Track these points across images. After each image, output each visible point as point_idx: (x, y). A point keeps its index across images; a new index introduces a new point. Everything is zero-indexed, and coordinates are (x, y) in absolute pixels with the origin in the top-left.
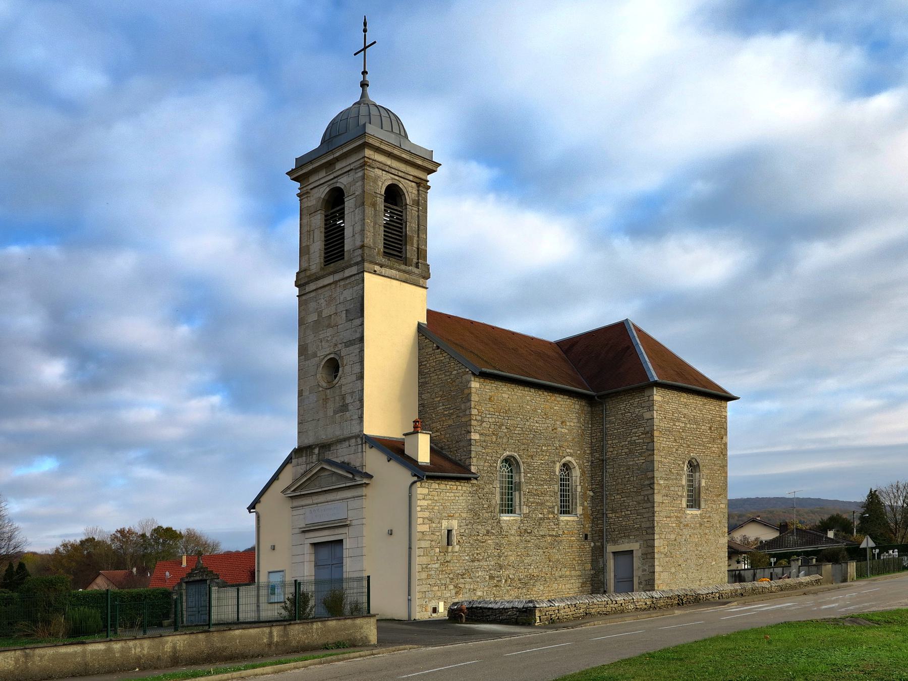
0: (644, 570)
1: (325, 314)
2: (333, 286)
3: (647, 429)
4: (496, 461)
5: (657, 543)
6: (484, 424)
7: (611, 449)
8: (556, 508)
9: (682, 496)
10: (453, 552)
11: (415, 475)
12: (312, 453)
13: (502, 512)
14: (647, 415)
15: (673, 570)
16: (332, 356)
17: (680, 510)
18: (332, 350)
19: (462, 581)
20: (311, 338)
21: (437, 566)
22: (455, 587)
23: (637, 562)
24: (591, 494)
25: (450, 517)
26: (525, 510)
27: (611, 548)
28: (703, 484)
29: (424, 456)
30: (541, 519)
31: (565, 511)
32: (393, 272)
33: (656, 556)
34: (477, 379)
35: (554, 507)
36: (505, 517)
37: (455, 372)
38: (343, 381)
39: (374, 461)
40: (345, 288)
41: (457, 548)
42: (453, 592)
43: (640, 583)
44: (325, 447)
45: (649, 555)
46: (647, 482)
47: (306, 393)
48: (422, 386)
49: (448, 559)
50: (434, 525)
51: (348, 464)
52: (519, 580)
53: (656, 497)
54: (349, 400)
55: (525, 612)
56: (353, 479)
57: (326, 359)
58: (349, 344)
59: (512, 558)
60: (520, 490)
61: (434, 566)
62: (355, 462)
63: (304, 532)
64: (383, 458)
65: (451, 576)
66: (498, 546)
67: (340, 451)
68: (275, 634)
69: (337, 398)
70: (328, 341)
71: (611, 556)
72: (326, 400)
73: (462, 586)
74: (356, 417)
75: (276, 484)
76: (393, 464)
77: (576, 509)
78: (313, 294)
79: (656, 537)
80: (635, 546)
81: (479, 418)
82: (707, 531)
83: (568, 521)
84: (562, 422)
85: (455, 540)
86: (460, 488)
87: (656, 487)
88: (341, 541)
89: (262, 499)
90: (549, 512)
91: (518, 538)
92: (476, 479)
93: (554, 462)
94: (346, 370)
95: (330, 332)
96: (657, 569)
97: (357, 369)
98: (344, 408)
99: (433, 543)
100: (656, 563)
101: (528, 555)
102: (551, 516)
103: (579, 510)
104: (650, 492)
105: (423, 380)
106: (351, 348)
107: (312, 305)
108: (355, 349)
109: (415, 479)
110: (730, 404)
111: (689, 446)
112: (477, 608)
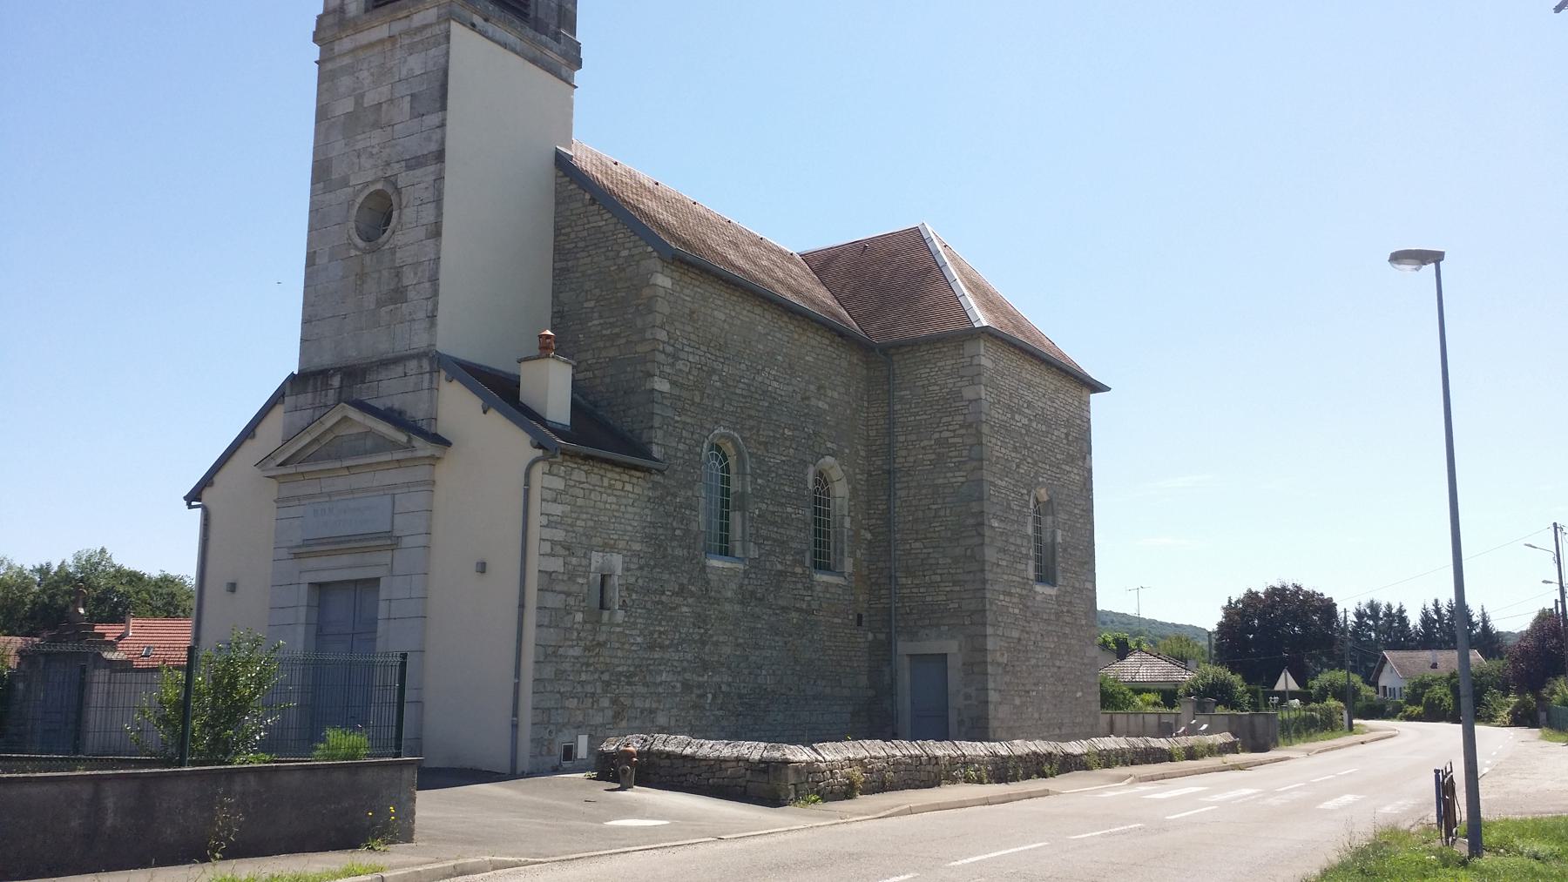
0: (968, 697)
1: (370, 99)
2: (388, 46)
3: (970, 419)
4: (700, 443)
5: (990, 645)
6: (680, 365)
7: (904, 453)
8: (808, 555)
9: (1027, 556)
10: (612, 624)
11: (539, 446)
12: (327, 386)
13: (708, 551)
14: (968, 393)
15: (1017, 701)
16: (379, 186)
17: (1025, 583)
18: (380, 174)
19: (628, 690)
20: (339, 146)
21: (577, 652)
22: (614, 701)
23: (955, 677)
24: (869, 536)
25: (608, 547)
26: (754, 552)
27: (904, 647)
28: (1059, 539)
29: (558, 409)
30: (780, 573)
31: (822, 565)
32: (511, 38)
33: (990, 669)
34: (667, 271)
35: (802, 552)
36: (715, 563)
37: (625, 253)
38: (399, 239)
39: (457, 407)
40: (411, 49)
41: (620, 616)
42: (610, 713)
43: (961, 723)
44: (354, 374)
45: (976, 665)
46: (971, 521)
47: (322, 260)
48: (561, 275)
49: (602, 638)
50: (574, 561)
51: (400, 413)
52: (740, 696)
53: (987, 551)
54: (409, 279)
55: (765, 771)
56: (409, 446)
57: (367, 192)
58: (414, 163)
59: (727, 650)
60: (742, 509)
61: (571, 652)
62: (417, 410)
63: (297, 556)
64: (475, 403)
65: (606, 677)
66: (701, 620)
67: (384, 384)
68: (110, 803)
69: (385, 273)
70: (372, 155)
71: (906, 661)
72: (362, 276)
73: (628, 702)
74: (422, 315)
75: (249, 444)
76: (494, 415)
77: (841, 561)
78: (347, 60)
79: (990, 630)
80: (951, 646)
81: (669, 349)
82: (1067, 630)
83: (828, 585)
84: (819, 388)
85: (615, 596)
86: (628, 487)
87: (987, 532)
88: (378, 580)
89: (217, 479)
90: (795, 562)
91: (737, 608)
92: (660, 472)
93: (805, 464)
94: (405, 236)
95: (376, 137)
96: (993, 696)
97: (428, 214)
98: (398, 295)
99: (571, 601)
100: (991, 685)
101: (757, 647)
102: (799, 570)
103: (848, 565)
104: (976, 540)
105: (563, 264)
106: (419, 172)
107: (345, 82)
108: (426, 174)
109: (539, 452)
110: (1095, 398)
111: (1035, 463)
112: (660, 753)
